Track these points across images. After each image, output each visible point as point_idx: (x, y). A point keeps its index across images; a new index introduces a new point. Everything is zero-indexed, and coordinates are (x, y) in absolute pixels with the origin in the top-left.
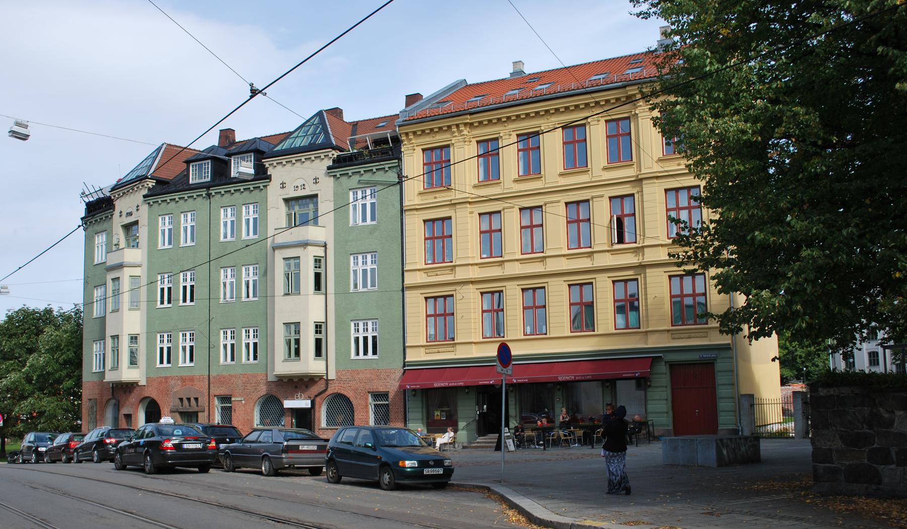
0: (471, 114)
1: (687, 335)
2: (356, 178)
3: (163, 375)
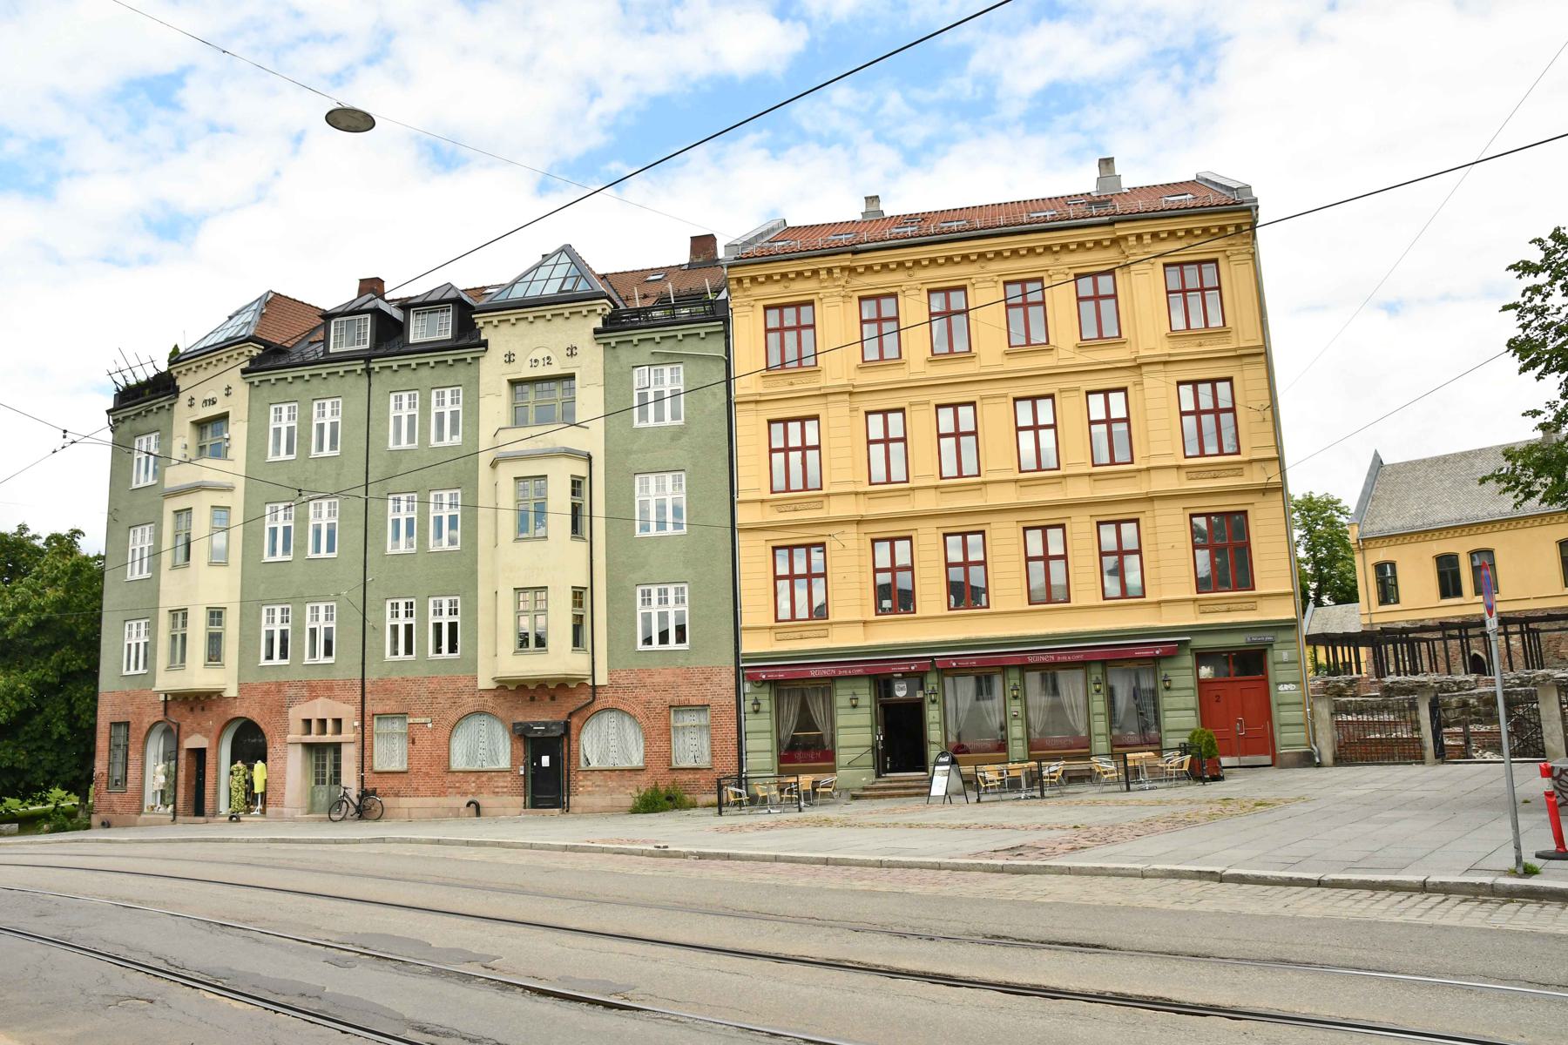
0: (854, 253)
1: (1225, 607)
2: (649, 348)
3: (273, 679)
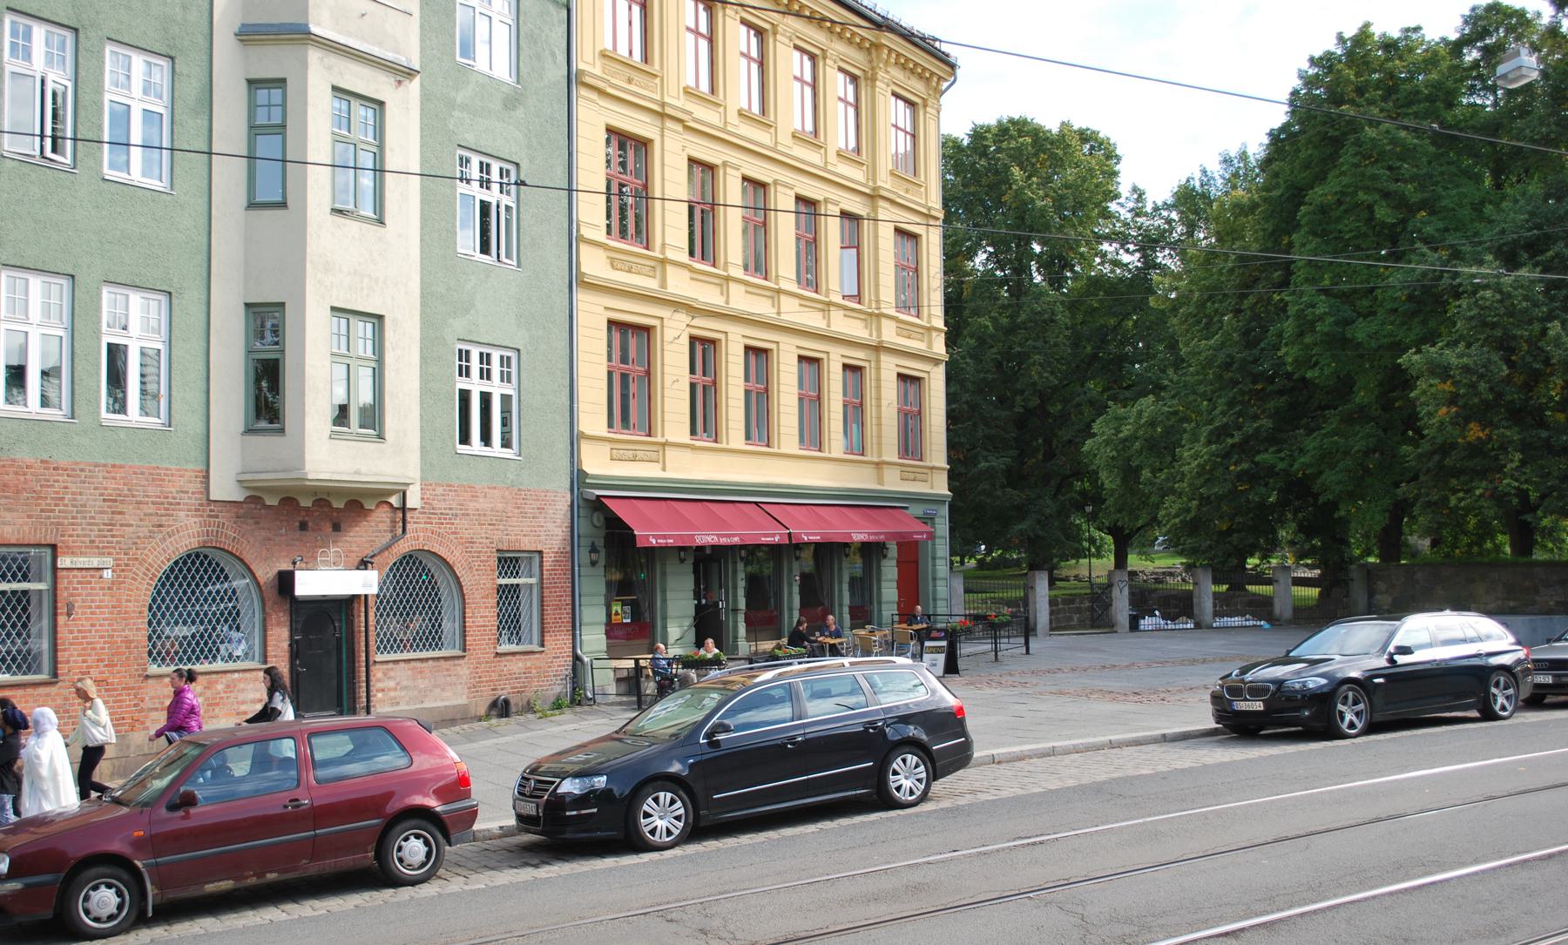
1: (912, 476)
